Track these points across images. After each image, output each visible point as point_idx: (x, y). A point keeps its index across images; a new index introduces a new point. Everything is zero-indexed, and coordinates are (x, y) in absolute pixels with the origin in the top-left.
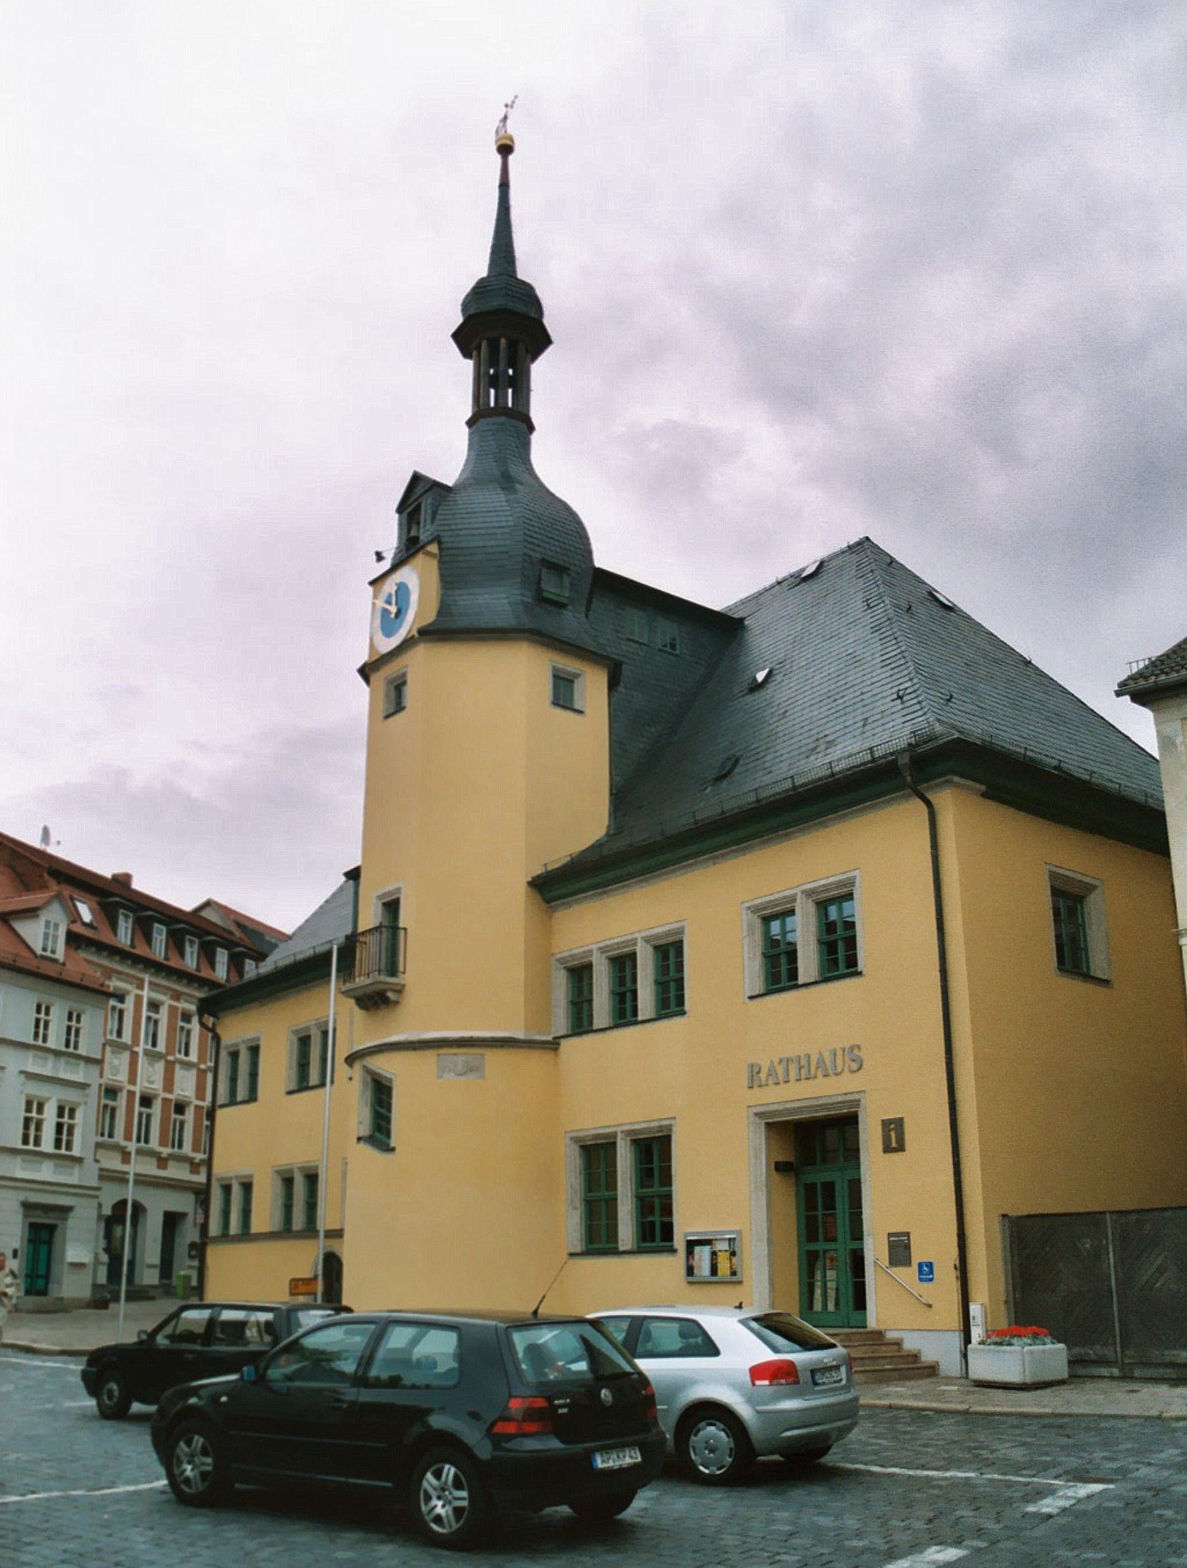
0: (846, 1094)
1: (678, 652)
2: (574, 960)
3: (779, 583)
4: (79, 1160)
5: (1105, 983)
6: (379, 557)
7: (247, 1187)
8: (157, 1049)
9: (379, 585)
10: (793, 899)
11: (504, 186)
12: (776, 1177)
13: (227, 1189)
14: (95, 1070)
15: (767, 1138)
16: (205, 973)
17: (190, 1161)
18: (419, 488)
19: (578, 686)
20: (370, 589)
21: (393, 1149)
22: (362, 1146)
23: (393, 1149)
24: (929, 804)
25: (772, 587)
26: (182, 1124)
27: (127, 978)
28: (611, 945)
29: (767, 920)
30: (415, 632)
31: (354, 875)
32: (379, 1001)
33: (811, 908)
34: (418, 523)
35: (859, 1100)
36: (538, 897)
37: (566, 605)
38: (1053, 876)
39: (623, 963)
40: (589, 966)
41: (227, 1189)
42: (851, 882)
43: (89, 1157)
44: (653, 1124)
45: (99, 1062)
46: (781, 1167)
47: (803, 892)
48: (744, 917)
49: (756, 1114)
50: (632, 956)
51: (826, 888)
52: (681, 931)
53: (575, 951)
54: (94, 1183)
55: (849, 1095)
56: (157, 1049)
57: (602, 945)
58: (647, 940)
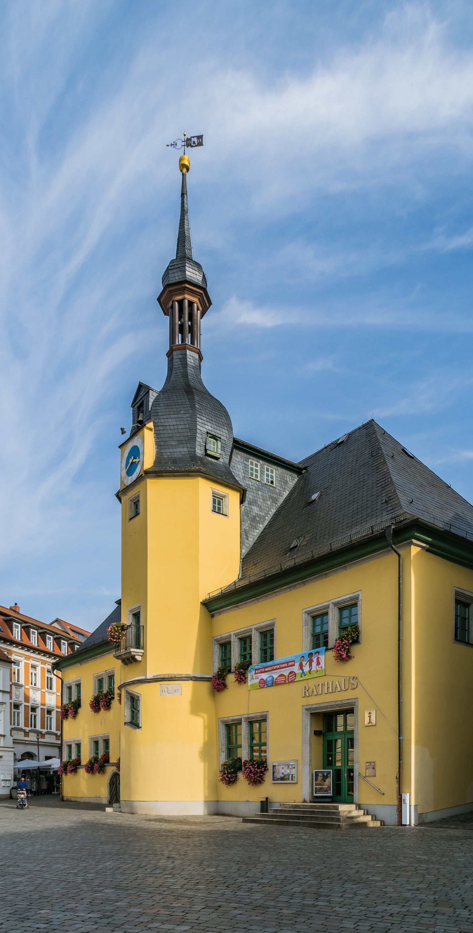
0: (349, 699)
1: (274, 486)
3: (326, 448)
6: (123, 432)
7: (79, 746)
9: (124, 447)
10: (327, 607)
11: (184, 150)
12: (314, 737)
13: (70, 746)
14: (8, 696)
15: (311, 720)
16: (57, 652)
18: (142, 392)
19: (225, 501)
20: (120, 450)
21: (141, 727)
22: (126, 726)
23: (141, 727)
24: (399, 555)
25: (322, 450)
26: (51, 719)
27: (21, 655)
28: (240, 632)
29: (314, 618)
30: (142, 473)
31: (119, 602)
32: (132, 661)
33: (336, 611)
34: (143, 412)
35: (355, 702)
37: (219, 458)
38: (457, 593)
40: (229, 643)
41: (70, 746)
42: (357, 598)
43: (8, 734)
44: (258, 714)
45: (10, 693)
46: (317, 733)
47: (333, 603)
48: (304, 616)
49: (306, 709)
51: (344, 601)
52: (273, 624)
53: (223, 636)
55: (350, 700)
57: (236, 632)
58: (236, 635)
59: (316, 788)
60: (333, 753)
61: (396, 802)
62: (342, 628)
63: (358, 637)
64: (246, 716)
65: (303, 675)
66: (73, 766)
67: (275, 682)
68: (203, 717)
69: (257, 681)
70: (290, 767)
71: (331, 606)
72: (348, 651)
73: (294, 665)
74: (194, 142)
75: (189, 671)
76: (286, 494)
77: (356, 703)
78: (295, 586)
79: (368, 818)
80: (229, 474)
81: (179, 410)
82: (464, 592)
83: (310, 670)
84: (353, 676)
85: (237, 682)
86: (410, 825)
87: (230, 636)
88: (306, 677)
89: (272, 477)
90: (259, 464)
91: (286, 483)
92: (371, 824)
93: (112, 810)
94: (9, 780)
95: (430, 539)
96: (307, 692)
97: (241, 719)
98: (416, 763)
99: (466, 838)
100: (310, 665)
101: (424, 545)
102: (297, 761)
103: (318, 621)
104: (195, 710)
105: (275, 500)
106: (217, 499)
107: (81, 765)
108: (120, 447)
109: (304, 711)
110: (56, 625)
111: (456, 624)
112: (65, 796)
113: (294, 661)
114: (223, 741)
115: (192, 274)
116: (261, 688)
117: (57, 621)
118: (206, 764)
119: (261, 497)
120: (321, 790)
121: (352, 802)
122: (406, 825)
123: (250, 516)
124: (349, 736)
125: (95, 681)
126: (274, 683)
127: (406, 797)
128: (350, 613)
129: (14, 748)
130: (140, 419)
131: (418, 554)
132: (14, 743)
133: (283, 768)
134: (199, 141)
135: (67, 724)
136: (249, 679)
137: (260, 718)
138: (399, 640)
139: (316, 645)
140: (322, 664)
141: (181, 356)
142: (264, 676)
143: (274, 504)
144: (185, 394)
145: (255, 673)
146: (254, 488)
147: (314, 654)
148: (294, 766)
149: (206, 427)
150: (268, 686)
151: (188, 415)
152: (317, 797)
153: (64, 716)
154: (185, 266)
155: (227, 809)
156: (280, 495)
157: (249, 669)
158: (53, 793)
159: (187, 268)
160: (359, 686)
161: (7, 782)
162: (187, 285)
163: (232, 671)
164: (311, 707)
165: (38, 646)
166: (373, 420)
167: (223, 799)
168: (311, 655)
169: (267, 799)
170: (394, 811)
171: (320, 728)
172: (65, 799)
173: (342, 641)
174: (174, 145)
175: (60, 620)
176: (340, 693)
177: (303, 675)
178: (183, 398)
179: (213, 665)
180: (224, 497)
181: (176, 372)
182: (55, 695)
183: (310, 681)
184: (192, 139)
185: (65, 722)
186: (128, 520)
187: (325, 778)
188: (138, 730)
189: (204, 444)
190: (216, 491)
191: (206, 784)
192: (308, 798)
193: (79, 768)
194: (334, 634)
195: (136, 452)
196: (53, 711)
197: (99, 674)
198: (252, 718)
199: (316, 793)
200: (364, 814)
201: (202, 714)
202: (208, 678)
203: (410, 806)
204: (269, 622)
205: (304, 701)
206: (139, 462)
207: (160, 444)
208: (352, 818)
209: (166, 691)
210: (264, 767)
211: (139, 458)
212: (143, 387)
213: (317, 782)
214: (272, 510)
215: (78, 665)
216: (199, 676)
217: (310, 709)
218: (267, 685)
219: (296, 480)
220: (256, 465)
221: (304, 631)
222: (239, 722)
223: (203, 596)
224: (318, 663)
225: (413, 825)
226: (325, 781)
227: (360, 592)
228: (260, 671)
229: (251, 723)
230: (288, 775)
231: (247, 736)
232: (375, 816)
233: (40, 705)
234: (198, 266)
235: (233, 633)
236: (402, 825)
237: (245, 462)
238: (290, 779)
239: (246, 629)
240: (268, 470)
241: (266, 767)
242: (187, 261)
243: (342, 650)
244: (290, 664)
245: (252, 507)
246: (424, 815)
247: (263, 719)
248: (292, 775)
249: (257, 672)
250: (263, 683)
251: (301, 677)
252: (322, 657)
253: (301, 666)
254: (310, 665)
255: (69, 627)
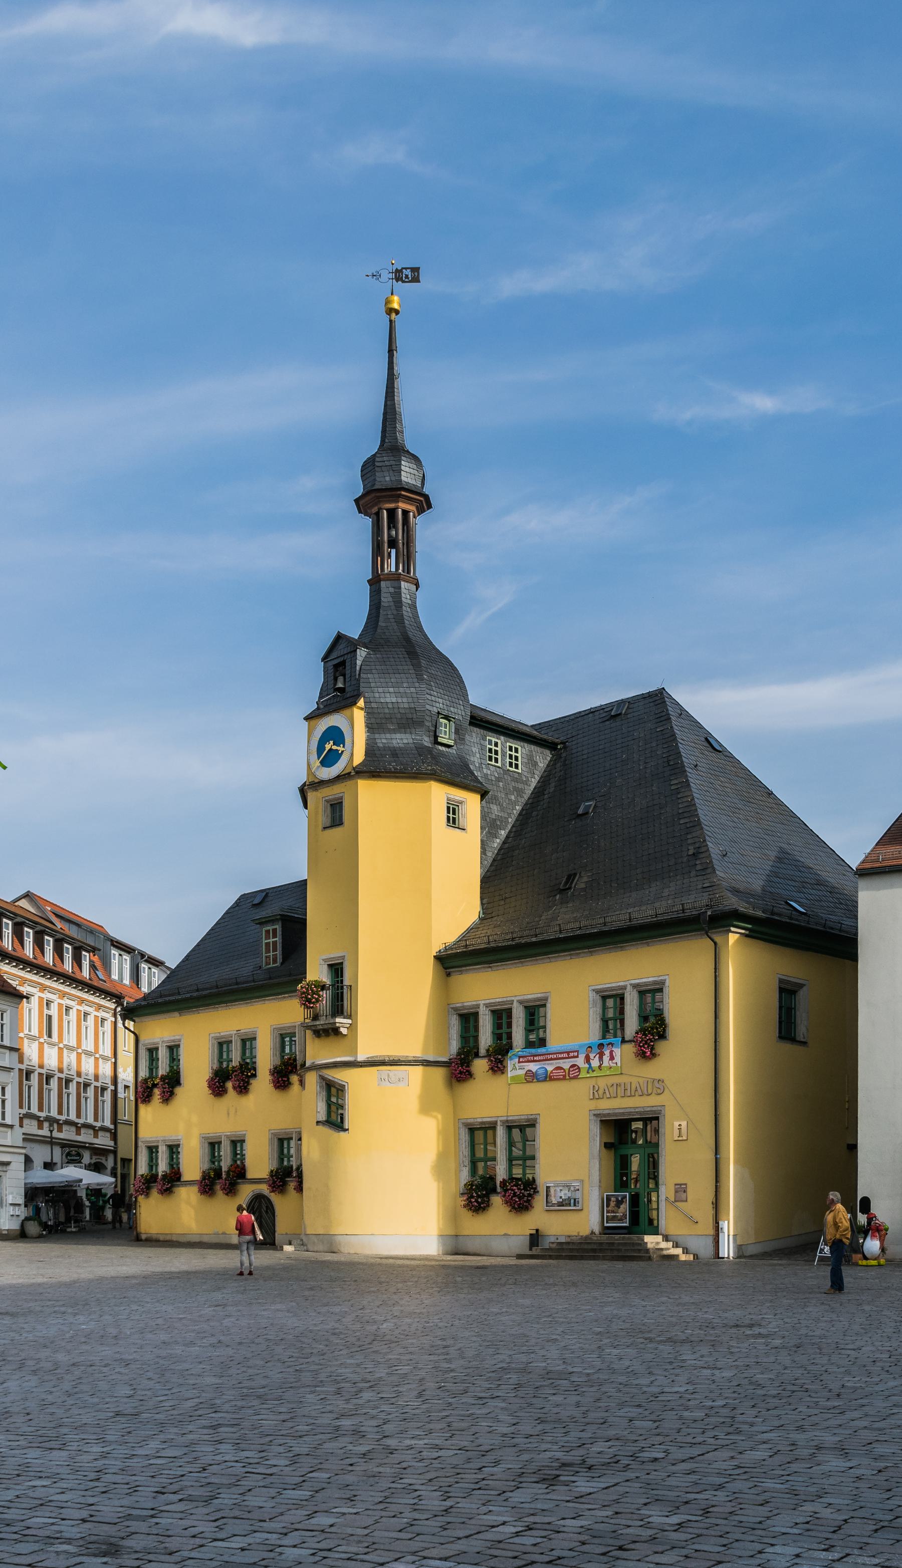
1: (520, 771)
2: (464, 1009)
4: (11, 1127)
5: (804, 1043)
8: (32, 1033)
15: (601, 1128)
17: (37, 1118)
19: (461, 810)
22: (320, 1127)
23: (348, 1130)
24: (715, 944)
29: (604, 998)
33: (635, 995)
34: (344, 675)
36: (439, 963)
38: (781, 981)
39: (502, 1016)
42: (663, 983)
44: (523, 1117)
46: (607, 1146)
47: (631, 984)
48: (591, 995)
49: (594, 1115)
50: (509, 1012)
51: (646, 984)
53: (466, 1004)
54: (20, 1144)
56: (53, 1040)
57: (488, 1002)
59: (607, 1216)
60: (629, 1171)
61: (712, 1232)
62: (644, 1018)
63: (664, 1030)
64: (505, 1118)
65: (590, 1071)
66: (168, 1183)
67: (550, 1077)
68: (435, 1117)
69: (523, 1072)
70: (572, 1188)
71: (629, 988)
72: (652, 1048)
73: (577, 1057)
74: (407, 276)
75: (415, 1050)
76: (534, 783)
77: (663, 1112)
78: (578, 954)
79: (678, 1251)
80: (465, 767)
81: (399, 680)
82: (789, 979)
83: (601, 1065)
84: (658, 1077)
85: (490, 1071)
86: (728, 1258)
87: (478, 1006)
88: (595, 1074)
89: (517, 758)
90: (499, 742)
91: (535, 764)
92: (683, 1258)
93: (293, 1249)
94: (19, 1205)
95: (750, 926)
96: (596, 1093)
97: (497, 1121)
98: (735, 1186)
99: (789, 1265)
100: (601, 1059)
101: (743, 931)
102: (583, 1181)
103: (610, 1003)
104: (426, 1108)
105: (520, 792)
106: (451, 806)
107: (182, 1180)
108: (306, 719)
109: (592, 1117)
110: (24, 903)
111: (780, 1018)
112: (143, 1231)
113: (578, 1051)
114: (466, 1152)
115: (408, 474)
116: (528, 1082)
117: (27, 896)
118: (441, 1184)
119: (502, 790)
120: (614, 1219)
121: (656, 1233)
122: (724, 1258)
123: (488, 820)
124: (650, 1150)
125: (213, 1045)
126: (548, 1078)
127: (724, 1225)
128: (653, 998)
129: (25, 1148)
130: (340, 685)
131: (737, 941)
132: (24, 1140)
133: (561, 1190)
134: (415, 275)
135: (145, 1112)
136: (509, 1069)
137: (526, 1122)
138: (715, 1042)
139: (605, 1031)
140: (617, 1059)
141: (392, 590)
142: (533, 1067)
143: (520, 800)
144: (407, 656)
145: (519, 1062)
146: (493, 778)
147: (606, 1046)
148: (577, 1188)
149: (437, 705)
150: (538, 1081)
151: (413, 690)
152: (608, 1228)
153: (146, 1098)
154: (401, 464)
155: (471, 1246)
156: (526, 783)
157: (509, 1055)
158: (69, 1230)
159: (403, 468)
160: (666, 1091)
161: (17, 1208)
162: (403, 493)
163: (481, 1055)
164: (601, 1112)
165: (35, 958)
166: (663, 688)
167: (466, 1232)
168: (601, 1046)
169: (537, 1230)
170: (710, 1241)
171: (611, 1140)
172: (143, 1237)
173: (644, 1034)
174: (376, 276)
175: (33, 894)
176: (641, 1097)
177: (590, 1071)
178: (404, 663)
179: (450, 1044)
180: (461, 802)
181: (385, 613)
182: (57, 1047)
183: (599, 1079)
184: (404, 270)
185: (143, 1109)
186: (320, 827)
187: (619, 1203)
188: (342, 1134)
189: (433, 729)
190: (452, 797)
191: (441, 1212)
192: (597, 1229)
193: (178, 1186)
194: (632, 1024)
195: (335, 735)
196: (33, 1072)
197: (222, 1034)
198: (513, 1121)
199: (607, 1223)
200: (673, 1247)
201: (435, 1114)
202: (444, 1062)
203: (729, 1235)
204: (539, 995)
205: (593, 1105)
206: (343, 752)
207: (371, 727)
208: (662, 1249)
209: (387, 1080)
210: (532, 1188)
211: (344, 747)
212: (344, 640)
213: (610, 1208)
214: (517, 808)
215: (176, 1014)
216: (432, 1059)
217: (600, 1114)
218: (537, 1079)
219: (549, 759)
220: (496, 745)
221: (591, 1013)
222: (490, 1127)
223: (437, 946)
224: (612, 1058)
225: (731, 1258)
226: (619, 1208)
227: (667, 977)
228: (525, 1059)
229: (509, 1128)
230: (569, 1199)
231: (504, 1146)
232: (687, 1249)
233: (37, 1067)
234: (416, 459)
235: (483, 1002)
236: (719, 1258)
237: (482, 742)
238: (572, 1204)
239: (505, 999)
240: (511, 749)
241: (535, 1189)
242: (403, 458)
243: (646, 1046)
244: (571, 1054)
245: (491, 805)
246: (743, 1247)
247: (531, 1124)
248: (575, 1200)
249: (521, 1060)
250: (531, 1076)
251: (588, 1072)
252: (617, 1052)
253: (588, 1059)
254: (601, 1059)
255: (49, 909)
